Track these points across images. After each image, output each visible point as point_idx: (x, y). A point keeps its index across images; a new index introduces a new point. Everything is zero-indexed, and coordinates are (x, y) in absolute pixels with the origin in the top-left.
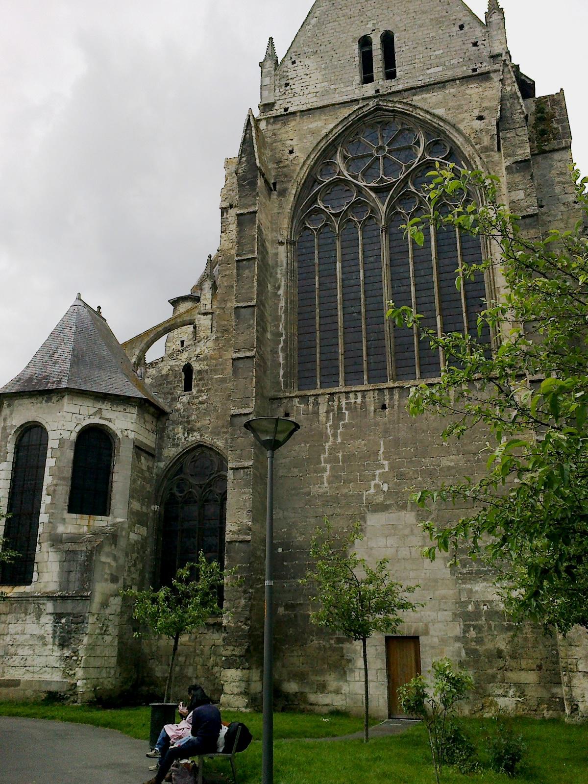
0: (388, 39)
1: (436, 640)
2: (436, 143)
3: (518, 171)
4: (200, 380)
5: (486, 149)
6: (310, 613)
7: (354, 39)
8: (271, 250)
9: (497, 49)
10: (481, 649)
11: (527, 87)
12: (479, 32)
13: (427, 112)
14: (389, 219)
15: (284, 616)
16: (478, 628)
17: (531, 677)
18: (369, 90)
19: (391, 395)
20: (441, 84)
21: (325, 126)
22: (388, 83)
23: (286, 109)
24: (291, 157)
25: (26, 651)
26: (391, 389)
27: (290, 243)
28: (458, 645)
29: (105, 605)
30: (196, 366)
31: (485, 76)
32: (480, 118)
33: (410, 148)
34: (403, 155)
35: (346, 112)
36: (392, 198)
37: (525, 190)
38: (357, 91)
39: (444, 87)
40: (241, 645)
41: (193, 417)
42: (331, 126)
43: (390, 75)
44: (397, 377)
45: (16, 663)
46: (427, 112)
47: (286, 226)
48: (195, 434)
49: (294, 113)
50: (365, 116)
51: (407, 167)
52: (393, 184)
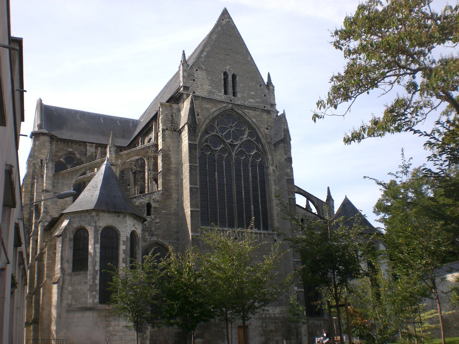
0: (234, 77)
1: (254, 327)
4: (156, 212)
16: (266, 323)
28: (260, 328)
30: (153, 205)
32: (267, 129)
41: (153, 229)
42: (214, 109)
43: (234, 94)
48: (154, 237)
52: (237, 145)
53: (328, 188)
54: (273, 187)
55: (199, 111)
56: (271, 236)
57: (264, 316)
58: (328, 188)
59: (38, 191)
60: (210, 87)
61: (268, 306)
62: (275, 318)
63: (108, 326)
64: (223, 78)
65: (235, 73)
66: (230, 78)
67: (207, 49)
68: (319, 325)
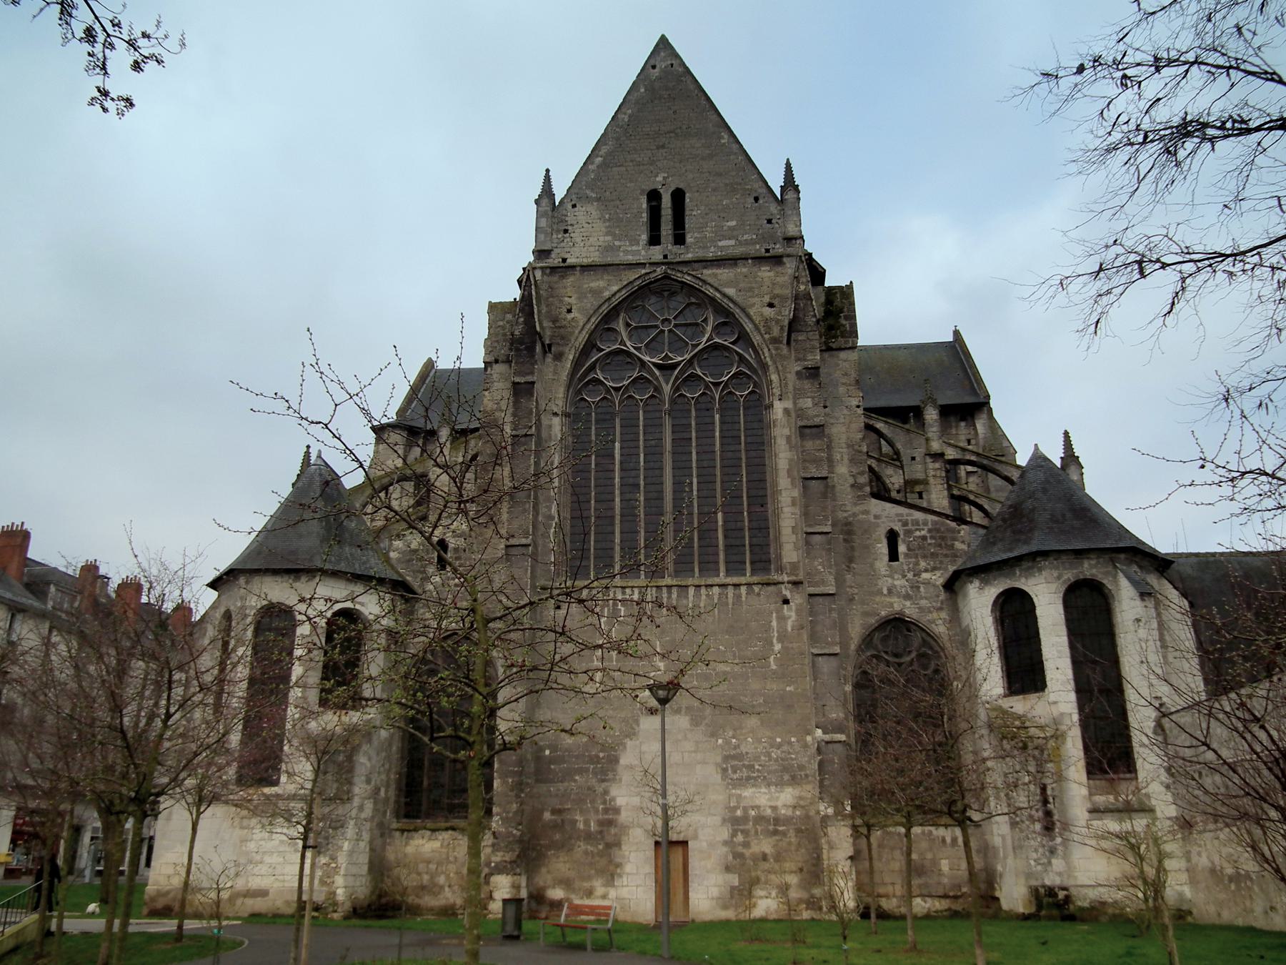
0: (678, 196)
2: (724, 324)
3: (807, 378)
5: (775, 341)
6: (577, 818)
7: (643, 191)
8: (545, 420)
9: (791, 230)
10: (747, 853)
11: (817, 274)
12: (774, 208)
13: (717, 290)
14: (673, 401)
15: (550, 821)
17: (793, 880)
18: (656, 253)
19: (670, 593)
20: (732, 261)
21: (611, 287)
22: (676, 249)
23: (564, 260)
24: (570, 316)
25: (275, 859)
26: (669, 587)
27: (567, 415)
29: (361, 808)
31: (777, 260)
32: (771, 305)
33: (697, 324)
34: (690, 331)
35: (632, 275)
36: (677, 378)
37: (813, 398)
38: (643, 253)
39: (736, 265)
40: (513, 850)
42: (615, 288)
43: (679, 239)
44: (677, 573)
45: (263, 872)
46: (717, 290)
47: (561, 395)
49: (573, 267)
50: (651, 283)
51: (695, 346)
52: (678, 364)
53: (1066, 434)
54: (781, 455)
55: (573, 301)
56: (771, 588)
57: (739, 813)
58: (1066, 434)
59: (755, 541)
60: (609, 238)
61: (753, 786)
62: (777, 821)
63: (244, 841)
64: (645, 206)
65: (681, 186)
66: (666, 201)
67: (604, 150)
68: (948, 840)
